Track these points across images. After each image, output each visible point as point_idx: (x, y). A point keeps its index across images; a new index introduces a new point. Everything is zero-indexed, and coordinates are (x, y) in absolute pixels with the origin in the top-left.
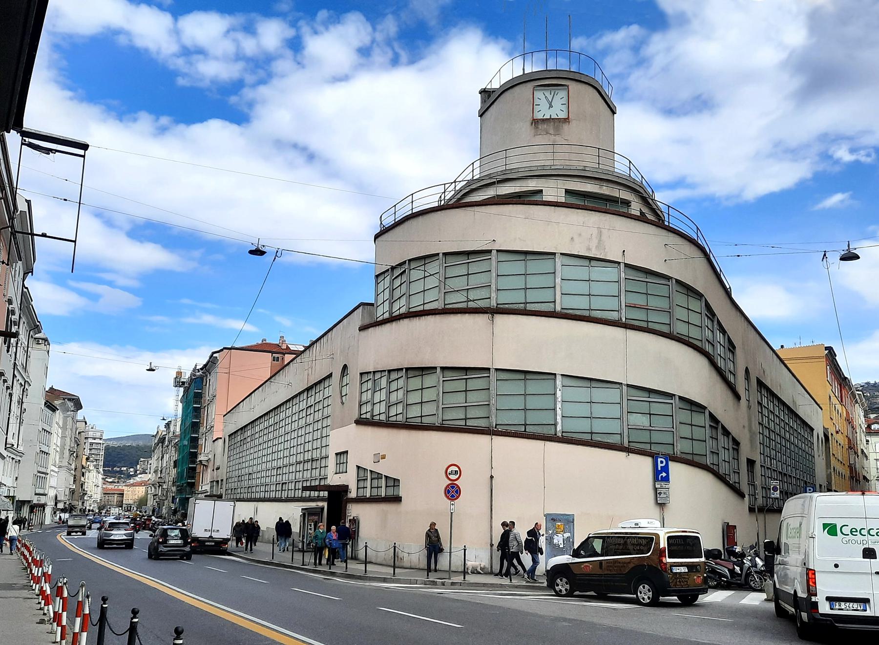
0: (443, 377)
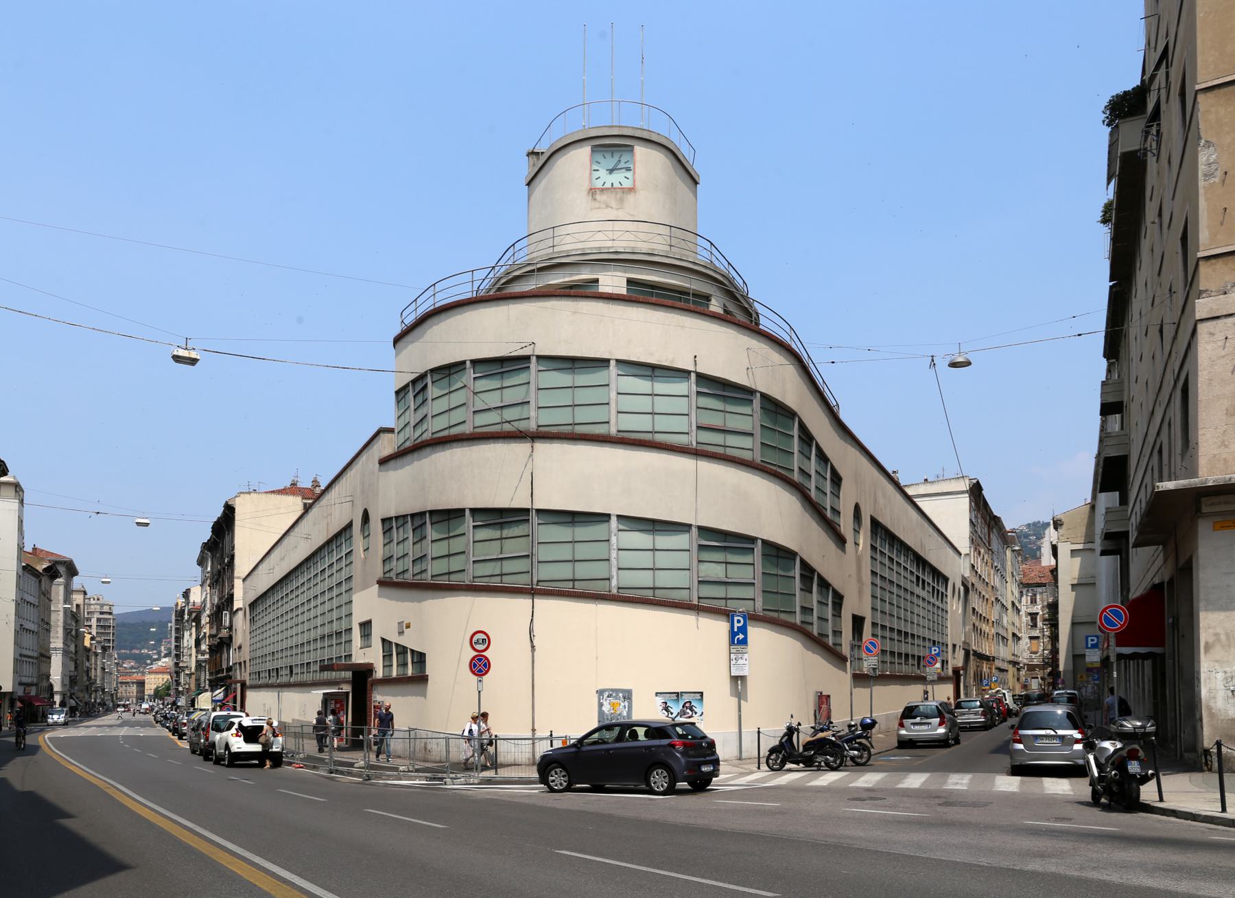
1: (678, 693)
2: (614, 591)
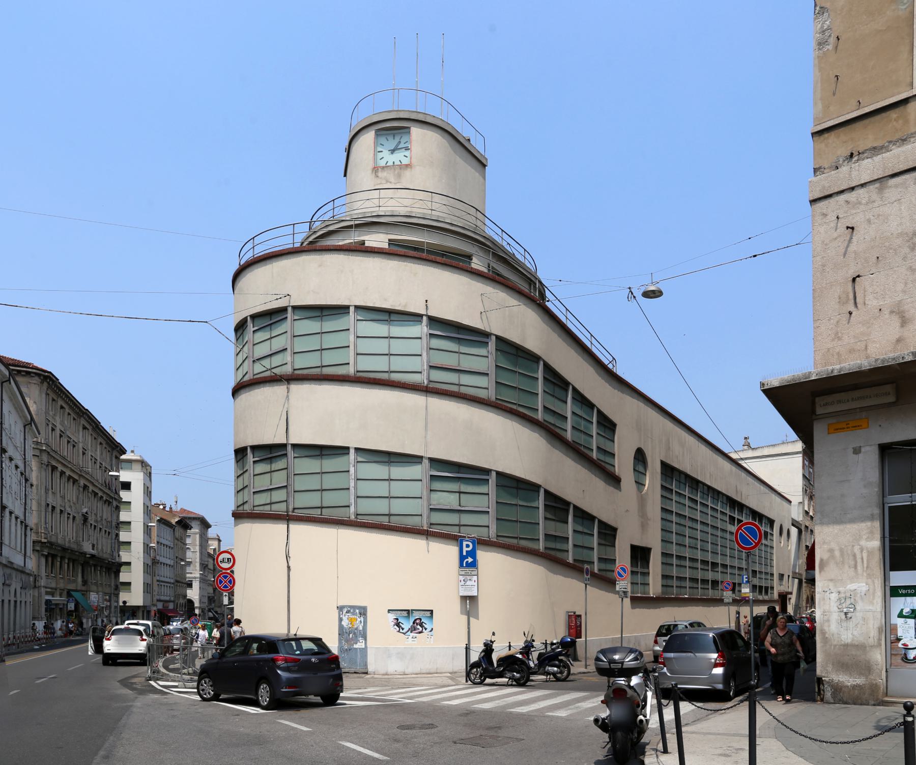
0: (253, 458)
1: (408, 611)
2: (353, 517)
